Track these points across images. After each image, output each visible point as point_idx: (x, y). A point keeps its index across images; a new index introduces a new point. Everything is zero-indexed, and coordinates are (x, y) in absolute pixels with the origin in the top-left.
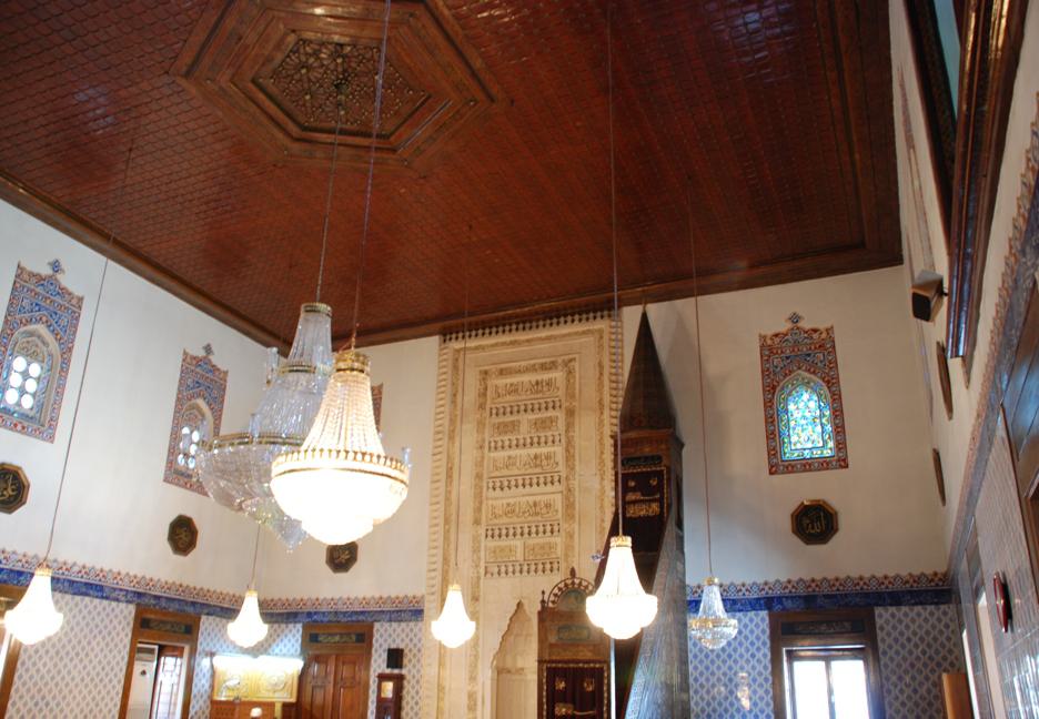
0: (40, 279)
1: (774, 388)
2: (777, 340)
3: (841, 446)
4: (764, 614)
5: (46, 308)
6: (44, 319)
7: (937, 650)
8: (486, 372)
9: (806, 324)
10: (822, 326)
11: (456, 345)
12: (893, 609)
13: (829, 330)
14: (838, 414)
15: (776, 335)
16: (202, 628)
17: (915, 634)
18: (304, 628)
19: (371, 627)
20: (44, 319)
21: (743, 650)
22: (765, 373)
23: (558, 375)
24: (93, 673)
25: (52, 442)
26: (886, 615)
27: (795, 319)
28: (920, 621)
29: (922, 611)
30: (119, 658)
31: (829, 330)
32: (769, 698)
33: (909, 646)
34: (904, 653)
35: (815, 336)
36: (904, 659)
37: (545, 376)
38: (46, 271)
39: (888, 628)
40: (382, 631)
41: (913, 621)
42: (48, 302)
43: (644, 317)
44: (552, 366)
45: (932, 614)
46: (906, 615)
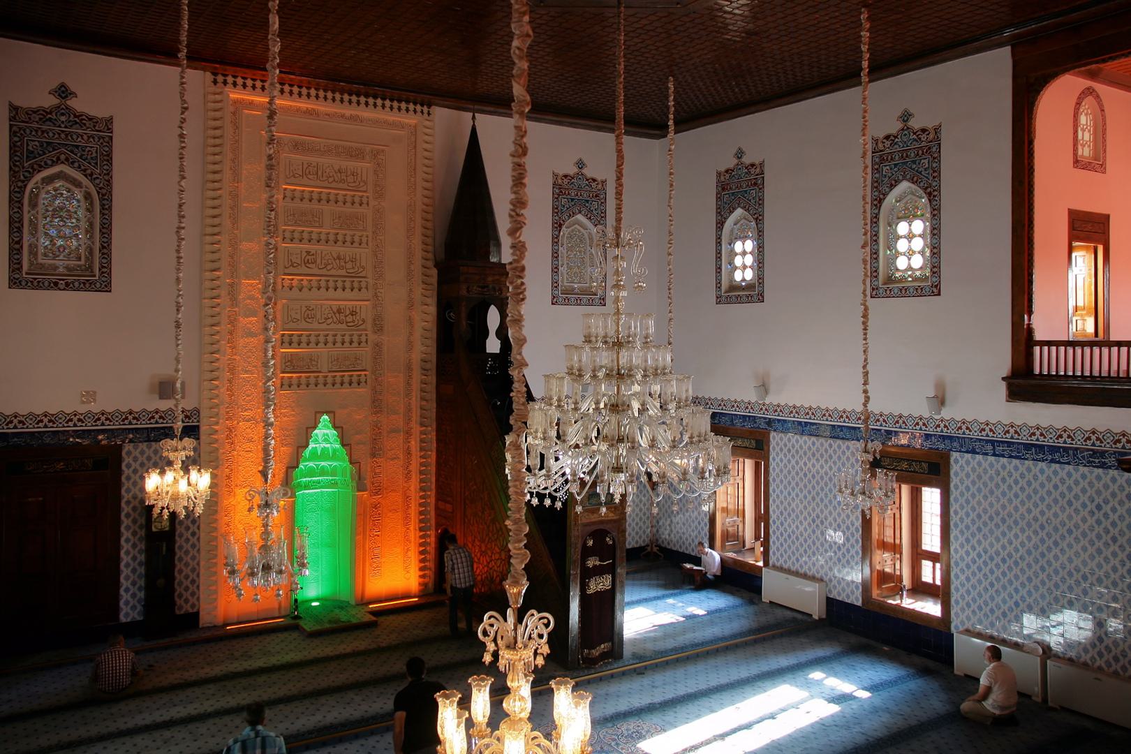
0: (44, 115)
1: (560, 226)
2: (566, 181)
5: (62, 142)
6: (63, 157)
9: (588, 172)
10: (599, 179)
15: (566, 176)
16: (773, 443)
20: (63, 157)
21: (1068, 482)
23: (364, 166)
25: (106, 287)
26: (777, 438)
27: (580, 164)
30: (778, 491)
35: (594, 185)
36: (1063, 495)
37: (351, 164)
38: (50, 101)
42: (63, 136)
44: (357, 154)
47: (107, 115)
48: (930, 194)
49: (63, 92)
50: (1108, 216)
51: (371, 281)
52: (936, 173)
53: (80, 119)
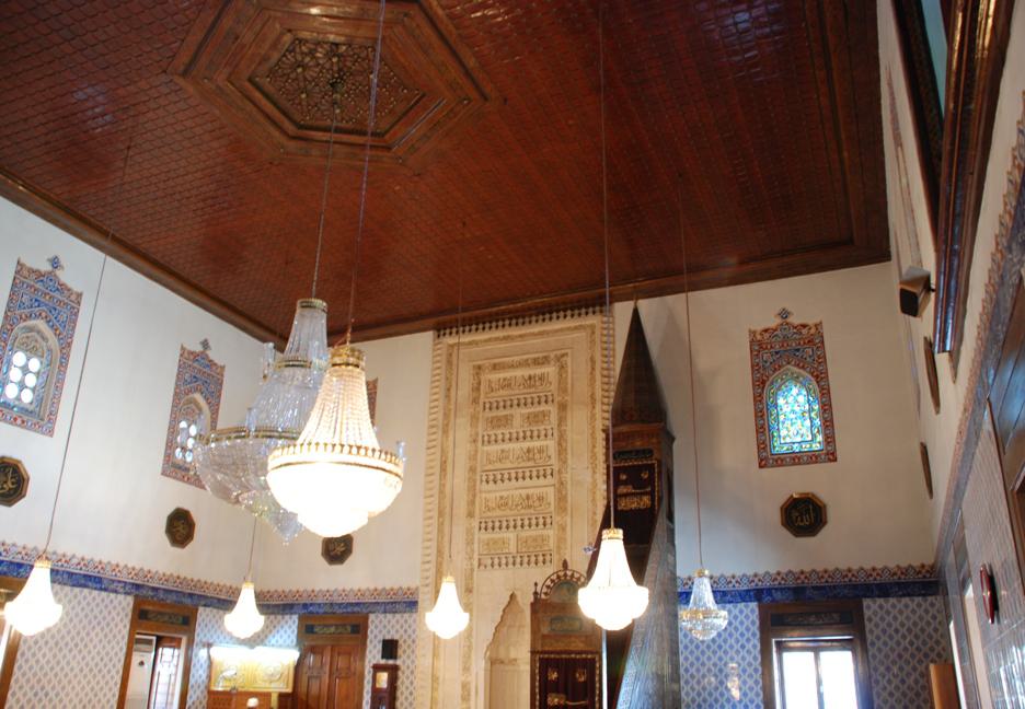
0: (39, 275)
1: (764, 382)
2: (767, 335)
3: (829, 439)
4: (754, 605)
5: (45, 303)
6: (44, 315)
7: (924, 641)
8: (479, 367)
9: (795, 320)
10: (811, 322)
11: (450, 340)
12: (881, 601)
13: (818, 326)
14: (826, 408)
15: (766, 331)
16: (199, 619)
17: (903, 625)
18: (300, 619)
19: (366, 619)
20: (44, 315)
21: (733, 641)
22: (755, 368)
23: (550, 370)
24: (92, 664)
25: (51, 436)
27: (784, 314)
28: (907, 612)
29: (909, 603)
30: (117, 649)
31: (818, 326)
32: (758, 688)
33: (897, 637)
34: (891, 644)
35: (804, 331)
37: (538, 371)
38: (45, 267)
39: (876, 619)
40: (377, 622)
41: (901, 612)
42: (47, 297)
43: (636, 313)
44: (545, 361)
45: (919, 605)
46: (894, 606)
47: (79, 291)
48: (817, 377)
49: (55, 262)
50: (164, 473)
51: (556, 468)
52: (822, 360)
53: (62, 288)
